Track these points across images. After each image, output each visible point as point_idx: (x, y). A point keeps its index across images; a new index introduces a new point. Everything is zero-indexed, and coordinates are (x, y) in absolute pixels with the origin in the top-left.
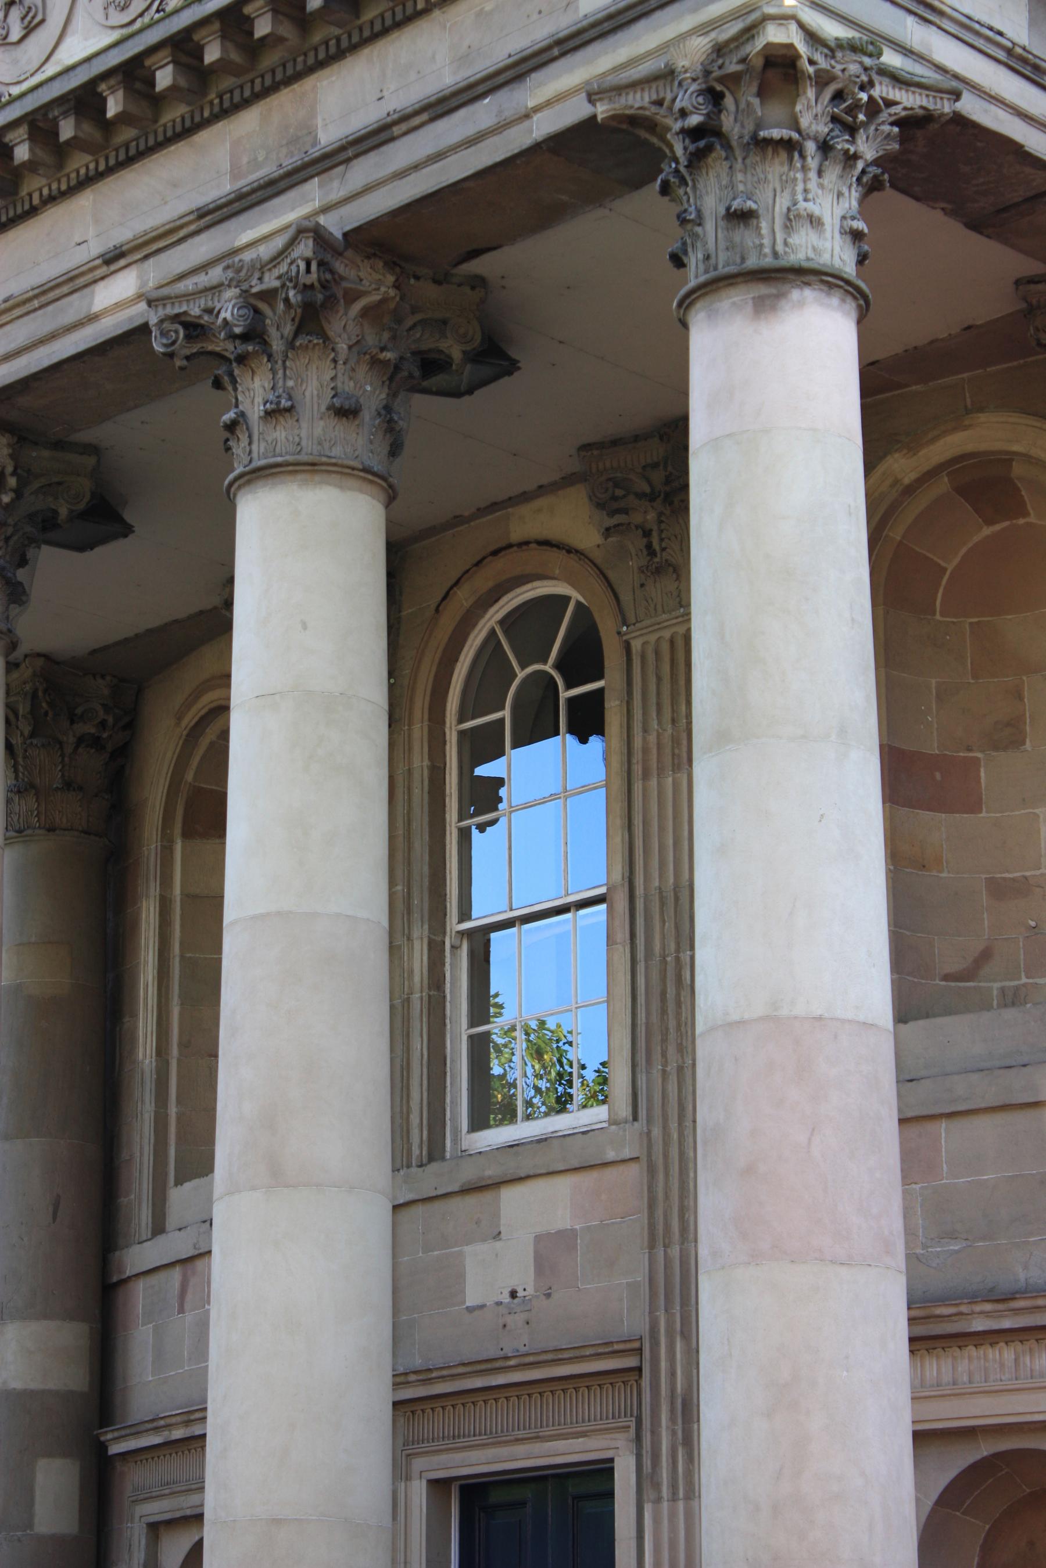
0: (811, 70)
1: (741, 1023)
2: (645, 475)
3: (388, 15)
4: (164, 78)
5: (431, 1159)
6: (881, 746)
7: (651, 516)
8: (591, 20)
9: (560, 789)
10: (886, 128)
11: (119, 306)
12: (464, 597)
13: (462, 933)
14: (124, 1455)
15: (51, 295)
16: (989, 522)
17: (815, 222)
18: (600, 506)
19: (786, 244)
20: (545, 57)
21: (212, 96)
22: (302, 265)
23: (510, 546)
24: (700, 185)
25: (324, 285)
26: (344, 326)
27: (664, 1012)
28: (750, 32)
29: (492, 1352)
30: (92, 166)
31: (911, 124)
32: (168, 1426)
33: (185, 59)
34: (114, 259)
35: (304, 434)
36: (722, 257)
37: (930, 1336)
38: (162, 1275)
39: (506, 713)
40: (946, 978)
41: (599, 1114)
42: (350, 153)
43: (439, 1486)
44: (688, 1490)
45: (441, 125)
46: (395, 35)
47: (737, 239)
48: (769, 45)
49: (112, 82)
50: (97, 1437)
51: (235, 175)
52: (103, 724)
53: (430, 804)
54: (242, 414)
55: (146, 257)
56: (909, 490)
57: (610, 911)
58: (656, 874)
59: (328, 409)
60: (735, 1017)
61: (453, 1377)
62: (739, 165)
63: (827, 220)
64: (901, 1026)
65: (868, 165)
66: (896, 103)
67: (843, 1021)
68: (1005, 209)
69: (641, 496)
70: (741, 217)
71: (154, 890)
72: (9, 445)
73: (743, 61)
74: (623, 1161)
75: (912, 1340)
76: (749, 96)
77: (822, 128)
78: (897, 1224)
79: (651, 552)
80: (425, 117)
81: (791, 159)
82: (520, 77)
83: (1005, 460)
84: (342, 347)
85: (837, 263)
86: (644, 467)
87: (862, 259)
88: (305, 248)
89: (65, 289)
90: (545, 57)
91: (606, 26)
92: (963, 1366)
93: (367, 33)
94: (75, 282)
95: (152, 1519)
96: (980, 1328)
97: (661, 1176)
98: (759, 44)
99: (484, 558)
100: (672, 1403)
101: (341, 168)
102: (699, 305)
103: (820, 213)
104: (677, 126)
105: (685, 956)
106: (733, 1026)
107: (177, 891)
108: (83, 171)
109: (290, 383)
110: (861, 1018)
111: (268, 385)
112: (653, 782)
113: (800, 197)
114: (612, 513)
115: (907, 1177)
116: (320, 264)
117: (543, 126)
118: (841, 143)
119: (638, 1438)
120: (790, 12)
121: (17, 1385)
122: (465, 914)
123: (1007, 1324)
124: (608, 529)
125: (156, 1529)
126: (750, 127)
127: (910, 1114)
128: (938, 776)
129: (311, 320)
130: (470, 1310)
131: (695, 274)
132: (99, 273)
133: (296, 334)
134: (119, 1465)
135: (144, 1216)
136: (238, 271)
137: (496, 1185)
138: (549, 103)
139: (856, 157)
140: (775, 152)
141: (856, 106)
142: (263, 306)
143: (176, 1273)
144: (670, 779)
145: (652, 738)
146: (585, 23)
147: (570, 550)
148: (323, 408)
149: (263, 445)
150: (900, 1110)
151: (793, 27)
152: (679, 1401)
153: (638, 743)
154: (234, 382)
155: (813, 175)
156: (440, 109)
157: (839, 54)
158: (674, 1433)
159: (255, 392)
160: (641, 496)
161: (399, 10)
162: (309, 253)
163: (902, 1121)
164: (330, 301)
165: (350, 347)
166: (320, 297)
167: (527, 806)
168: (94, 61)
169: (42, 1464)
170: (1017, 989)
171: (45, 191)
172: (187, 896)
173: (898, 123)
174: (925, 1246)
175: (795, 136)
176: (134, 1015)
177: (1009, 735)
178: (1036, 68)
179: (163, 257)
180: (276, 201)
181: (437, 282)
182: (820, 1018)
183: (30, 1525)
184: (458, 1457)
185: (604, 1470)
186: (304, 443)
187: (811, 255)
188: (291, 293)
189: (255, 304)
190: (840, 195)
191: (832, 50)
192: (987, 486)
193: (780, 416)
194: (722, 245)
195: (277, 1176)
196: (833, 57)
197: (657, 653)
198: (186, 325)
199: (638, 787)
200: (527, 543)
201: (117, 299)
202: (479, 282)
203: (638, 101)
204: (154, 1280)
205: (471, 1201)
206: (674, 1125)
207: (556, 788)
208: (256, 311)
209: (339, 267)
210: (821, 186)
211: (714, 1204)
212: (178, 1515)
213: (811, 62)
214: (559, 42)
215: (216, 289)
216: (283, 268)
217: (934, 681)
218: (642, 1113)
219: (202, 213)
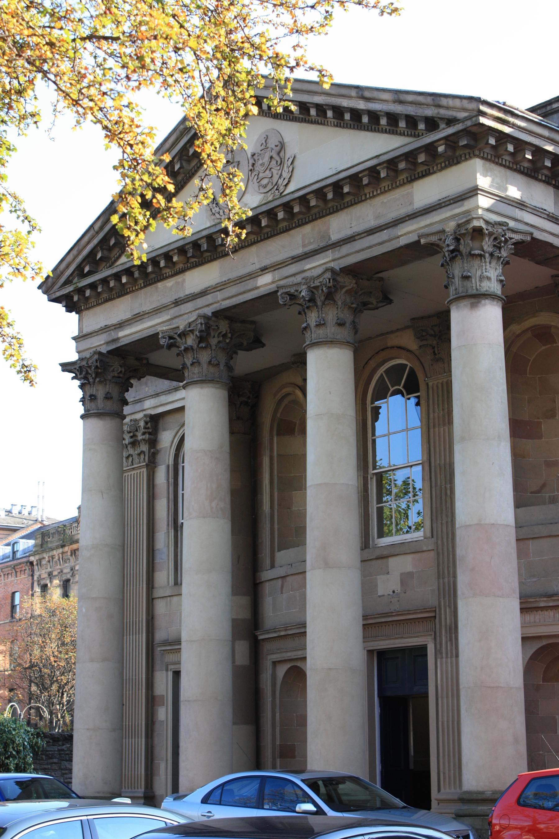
0: (487, 232)
1: (470, 525)
3: (353, 200)
4: (281, 215)
5: (366, 548)
6: (510, 419)
7: (435, 342)
8: (418, 210)
9: (405, 428)
10: (510, 246)
11: (266, 285)
12: (372, 364)
13: (374, 474)
15: (243, 279)
16: (544, 345)
17: (489, 279)
18: (418, 338)
19: (480, 286)
23: (388, 348)
24: (453, 266)
25: (334, 286)
26: (340, 297)
27: (441, 503)
28: (468, 222)
29: (387, 610)
30: (256, 239)
32: (279, 631)
33: (287, 209)
34: (264, 270)
35: (328, 331)
36: (461, 290)
37: (527, 607)
38: (275, 581)
40: (532, 493)
42: (341, 243)
45: (371, 237)
46: (355, 206)
47: (465, 284)
49: (263, 215)
50: (254, 634)
51: (304, 246)
52: (249, 397)
53: (363, 432)
54: (308, 325)
55: (275, 270)
56: (519, 336)
58: (438, 459)
59: (336, 323)
60: (468, 523)
61: (375, 618)
62: (465, 261)
63: (492, 278)
64: (517, 509)
68: (547, 259)
69: (431, 335)
71: (267, 453)
72: (228, 324)
73: (467, 229)
74: (429, 550)
75: (521, 609)
77: (491, 249)
78: (517, 584)
79: (435, 354)
80: (365, 234)
81: (481, 259)
82: (396, 225)
83: (549, 327)
86: (432, 326)
88: (328, 275)
89: (248, 278)
90: (404, 220)
91: (423, 212)
92: (537, 617)
93: (346, 205)
94: (252, 276)
96: (542, 605)
97: (441, 556)
98: (471, 225)
99: (379, 352)
100: (446, 628)
101: (339, 248)
102: (454, 304)
104: (447, 249)
106: (467, 526)
107: (275, 453)
108: (253, 240)
109: (324, 315)
110: (505, 523)
111: (317, 316)
112: (437, 429)
113: (484, 271)
114: (422, 341)
115: (519, 557)
116: (333, 280)
120: (480, 216)
122: (374, 468)
123: (551, 604)
124: (421, 346)
125: (275, 663)
126: (468, 250)
127: (520, 538)
128: (528, 427)
129: (330, 296)
130: (380, 596)
133: (326, 299)
135: (268, 562)
136: (306, 280)
137: (387, 557)
138: (405, 234)
139: (501, 257)
140: (476, 257)
141: (501, 242)
142: (314, 290)
143: (280, 582)
144: (442, 429)
145: (436, 415)
146: (416, 211)
147: (408, 350)
148: (334, 323)
149: (315, 335)
150: (517, 536)
151: (482, 220)
152: (448, 627)
153: (431, 416)
155: (488, 264)
156: (370, 233)
157: (495, 226)
158: (447, 637)
159: (312, 318)
160: (431, 335)
161: (356, 199)
162: (329, 277)
163: (517, 540)
164: (336, 291)
166: (333, 290)
167: (394, 433)
168: (258, 209)
170: (554, 496)
172: (279, 455)
173: (514, 244)
174: (525, 580)
175: (482, 253)
176: (262, 494)
177: (551, 414)
178: (557, 219)
180: (317, 256)
181: (368, 280)
182: (493, 524)
184: (376, 643)
186: (328, 335)
187: (488, 289)
188: (324, 289)
189: (312, 290)
190: (496, 269)
192: (543, 334)
193: (480, 336)
194: (460, 285)
195: (327, 565)
197: (437, 387)
198: (289, 295)
199: (432, 430)
200: (393, 347)
201: (265, 282)
202: (381, 279)
203: (434, 239)
204: (272, 582)
205: (379, 561)
206: (445, 540)
207: (405, 428)
208: (313, 292)
209: (339, 279)
210: (490, 267)
211: (462, 580)
212: (283, 659)
214: (408, 216)
216: (321, 280)
217: (527, 397)
219: (293, 258)
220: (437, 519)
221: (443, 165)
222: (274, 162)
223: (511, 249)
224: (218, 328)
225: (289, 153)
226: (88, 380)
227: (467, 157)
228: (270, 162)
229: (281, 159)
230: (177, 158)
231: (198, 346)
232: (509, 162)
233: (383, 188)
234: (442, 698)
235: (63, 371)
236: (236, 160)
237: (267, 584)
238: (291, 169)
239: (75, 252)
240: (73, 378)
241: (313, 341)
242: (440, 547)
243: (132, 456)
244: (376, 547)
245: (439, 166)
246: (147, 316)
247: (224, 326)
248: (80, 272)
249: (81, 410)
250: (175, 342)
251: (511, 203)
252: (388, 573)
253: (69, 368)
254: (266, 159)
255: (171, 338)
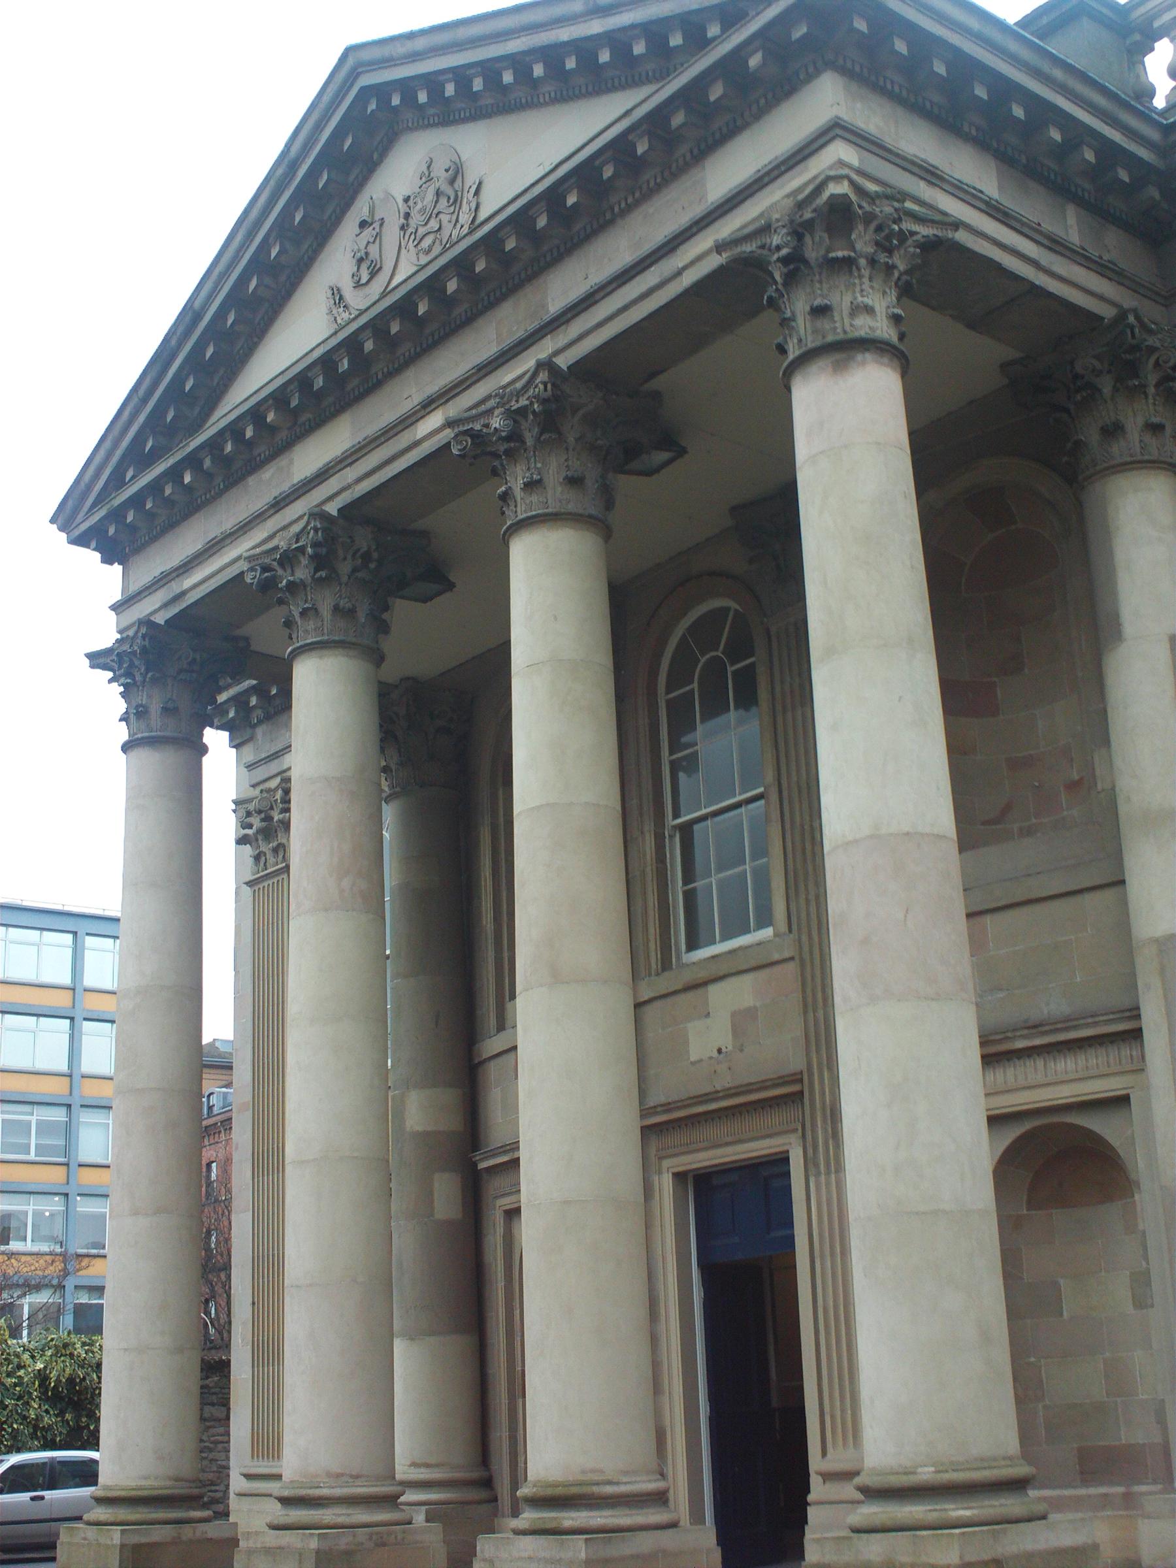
0: (860, 212)
2: (770, 525)
5: (664, 969)
10: (912, 250)
13: (674, 827)
14: (489, 1170)
15: (391, 433)
17: (869, 310)
19: (852, 325)
20: (688, 234)
21: (483, 294)
22: (541, 386)
26: (572, 430)
31: (930, 246)
34: (428, 405)
39: (695, 685)
41: (768, 932)
42: (569, 315)
43: (676, 1175)
44: (837, 1165)
48: (832, 195)
57: (767, 803)
58: (794, 773)
63: (877, 308)
65: (901, 274)
66: (916, 233)
67: (922, 835)
70: (820, 311)
76: (821, 234)
77: (870, 250)
80: (614, 285)
81: (851, 272)
84: (571, 440)
85: (886, 336)
87: (902, 337)
88: (543, 376)
89: (400, 428)
95: (508, 1207)
98: (826, 195)
103: (872, 307)
104: (775, 257)
105: (816, 824)
110: (936, 831)
116: (553, 385)
117: (689, 278)
118: (883, 258)
119: (804, 1136)
121: (420, 1128)
123: (1037, 1042)
126: (822, 252)
130: (693, 1063)
131: (793, 352)
132: (419, 415)
134: (485, 1176)
141: (891, 234)
142: (518, 418)
144: (799, 712)
154: (504, 469)
157: (877, 202)
159: (517, 477)
165: (577, 440)
169: (437, 1176)
171: (385, 370)
173: (918, 245)
175: (853, 254)
179: (458, 399)
182: (908, 834)
183: (432, 1215)
185: (782, 1160)
190: (884, 293)
191: (873, 199)
194: (809, 331)
196: (874, 204)
198: (473, 437)
203: (748, 248)
205: (690, 995)
210: (872, 287)
213: (860, 207)
215: (490, 412)
218: (795, 927)
220: (797, 891)
221: (762, 101)
222: (443, 202)
223: (914, 254)
224: (353, 541)
225: (471, 180)
226: (134, 679)
227: (811, 69)
228: (437, 202)
229: (457, 196)
230: (274, 234)
231: (313, 577)
232: (900, 86)
233: (645, 186)
234: (822, 1257)
235: (92, 667)
236: (377, 218)
237: (492, 1063)
238: (473, 206)
239: (108, 444)
240: (110, 681)
241: (520, 517)
242: (806, 949)
243: (265, 854)
244: (682, 966)
245: (754, 107)
246: (228, 541)
247: (364, 539)
248: (117, 481)
249: (122, 733)
250: (274, 577)
251: (909, 167)
252: (708, 1015)
253: (102, 660)
254: (430, 196)
255: (265, 569)
